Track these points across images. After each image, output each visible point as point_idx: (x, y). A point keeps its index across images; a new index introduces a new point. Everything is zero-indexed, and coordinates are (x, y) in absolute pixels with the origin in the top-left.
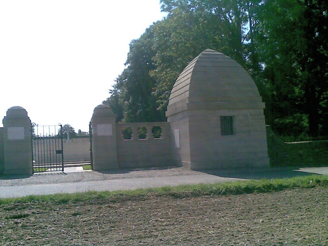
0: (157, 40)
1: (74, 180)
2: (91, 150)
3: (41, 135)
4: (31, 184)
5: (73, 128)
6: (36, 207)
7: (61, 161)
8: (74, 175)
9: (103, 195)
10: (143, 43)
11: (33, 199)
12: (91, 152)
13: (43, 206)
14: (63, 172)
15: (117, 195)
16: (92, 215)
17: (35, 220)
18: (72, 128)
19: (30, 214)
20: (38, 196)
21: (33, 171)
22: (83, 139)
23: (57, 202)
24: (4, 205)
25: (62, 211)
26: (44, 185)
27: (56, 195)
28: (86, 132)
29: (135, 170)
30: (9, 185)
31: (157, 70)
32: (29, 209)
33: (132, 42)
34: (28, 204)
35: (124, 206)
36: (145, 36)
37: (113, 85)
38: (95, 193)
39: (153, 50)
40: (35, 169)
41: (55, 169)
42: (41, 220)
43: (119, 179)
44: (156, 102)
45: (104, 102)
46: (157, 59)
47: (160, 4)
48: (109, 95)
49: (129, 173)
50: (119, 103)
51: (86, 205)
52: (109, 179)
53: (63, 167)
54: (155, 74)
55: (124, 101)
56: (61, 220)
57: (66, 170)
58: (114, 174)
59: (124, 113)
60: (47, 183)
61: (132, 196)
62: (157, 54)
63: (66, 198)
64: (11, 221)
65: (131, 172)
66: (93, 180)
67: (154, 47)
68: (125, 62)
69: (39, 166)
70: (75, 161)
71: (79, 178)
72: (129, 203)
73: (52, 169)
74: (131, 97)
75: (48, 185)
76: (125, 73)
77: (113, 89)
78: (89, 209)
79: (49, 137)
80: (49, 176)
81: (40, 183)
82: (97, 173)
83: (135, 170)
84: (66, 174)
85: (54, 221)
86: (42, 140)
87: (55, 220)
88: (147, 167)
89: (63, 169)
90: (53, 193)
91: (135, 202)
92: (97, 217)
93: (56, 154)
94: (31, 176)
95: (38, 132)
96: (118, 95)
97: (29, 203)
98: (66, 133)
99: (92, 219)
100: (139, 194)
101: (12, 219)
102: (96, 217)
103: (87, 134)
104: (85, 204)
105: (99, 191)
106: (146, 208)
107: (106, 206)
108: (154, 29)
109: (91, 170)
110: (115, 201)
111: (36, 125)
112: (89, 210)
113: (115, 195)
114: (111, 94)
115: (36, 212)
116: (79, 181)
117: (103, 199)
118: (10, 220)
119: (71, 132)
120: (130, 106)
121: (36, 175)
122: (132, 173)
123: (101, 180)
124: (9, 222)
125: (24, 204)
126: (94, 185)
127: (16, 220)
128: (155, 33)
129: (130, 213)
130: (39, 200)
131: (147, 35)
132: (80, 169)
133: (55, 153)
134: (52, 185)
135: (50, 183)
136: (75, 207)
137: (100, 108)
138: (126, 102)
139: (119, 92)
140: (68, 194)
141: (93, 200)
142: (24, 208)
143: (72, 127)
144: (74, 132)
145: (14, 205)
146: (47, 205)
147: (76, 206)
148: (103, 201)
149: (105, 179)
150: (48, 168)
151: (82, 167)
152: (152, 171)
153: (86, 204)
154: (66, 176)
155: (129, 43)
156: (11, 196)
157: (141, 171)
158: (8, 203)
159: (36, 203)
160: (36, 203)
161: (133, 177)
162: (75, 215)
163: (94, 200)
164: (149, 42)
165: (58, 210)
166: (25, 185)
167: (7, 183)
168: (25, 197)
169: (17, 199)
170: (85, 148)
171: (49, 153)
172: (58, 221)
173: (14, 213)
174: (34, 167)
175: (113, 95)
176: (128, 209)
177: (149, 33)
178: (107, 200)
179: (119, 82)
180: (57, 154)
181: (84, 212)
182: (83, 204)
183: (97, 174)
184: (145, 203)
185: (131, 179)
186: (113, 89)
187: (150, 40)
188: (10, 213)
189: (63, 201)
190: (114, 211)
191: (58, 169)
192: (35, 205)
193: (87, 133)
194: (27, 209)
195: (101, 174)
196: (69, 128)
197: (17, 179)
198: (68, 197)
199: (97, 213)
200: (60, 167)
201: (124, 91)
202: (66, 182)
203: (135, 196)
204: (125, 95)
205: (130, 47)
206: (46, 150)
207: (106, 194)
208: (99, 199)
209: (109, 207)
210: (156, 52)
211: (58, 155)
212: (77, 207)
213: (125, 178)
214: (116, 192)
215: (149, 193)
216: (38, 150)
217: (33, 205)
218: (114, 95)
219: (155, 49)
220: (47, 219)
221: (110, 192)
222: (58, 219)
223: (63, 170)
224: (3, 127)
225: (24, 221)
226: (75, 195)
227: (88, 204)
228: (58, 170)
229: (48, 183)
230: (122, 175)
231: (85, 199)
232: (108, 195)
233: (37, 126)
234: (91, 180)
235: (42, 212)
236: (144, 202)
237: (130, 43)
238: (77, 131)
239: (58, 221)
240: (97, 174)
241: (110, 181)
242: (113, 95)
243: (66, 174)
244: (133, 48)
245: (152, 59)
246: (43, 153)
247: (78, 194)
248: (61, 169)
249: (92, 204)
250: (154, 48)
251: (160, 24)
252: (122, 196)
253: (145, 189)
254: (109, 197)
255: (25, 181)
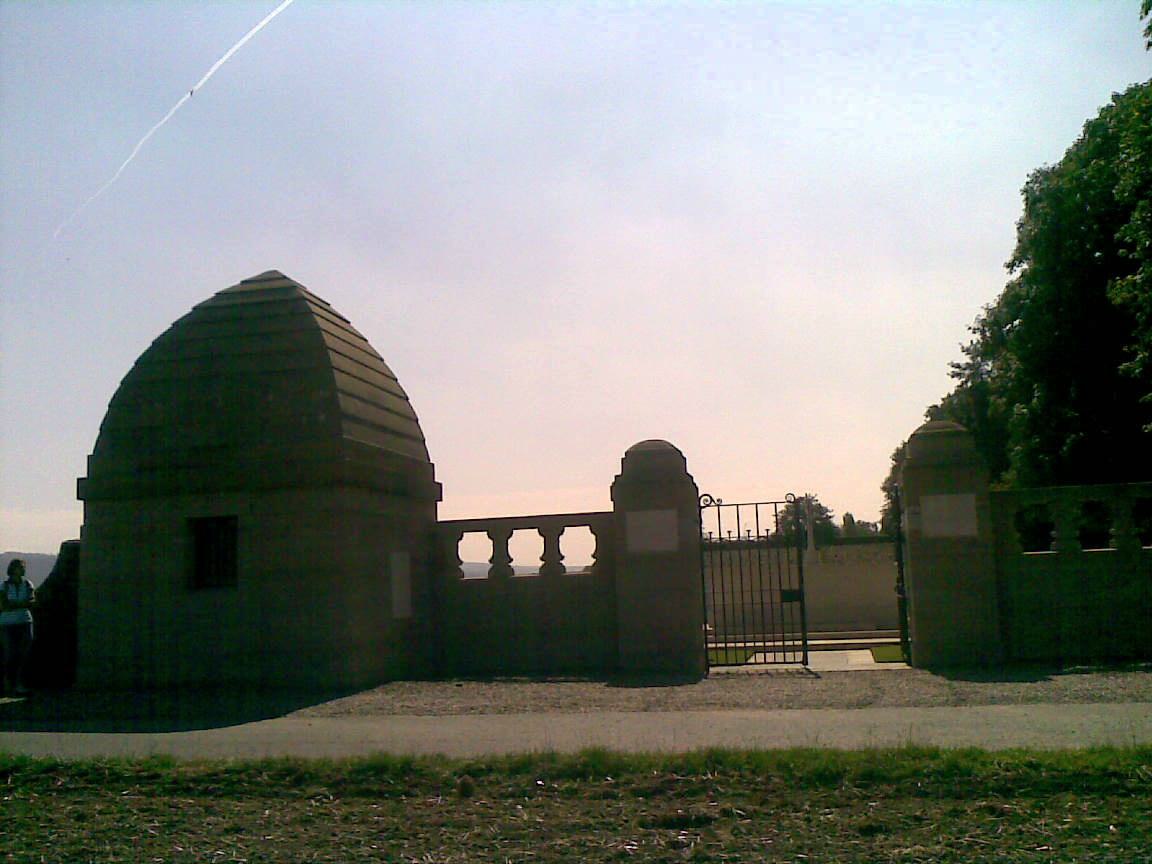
0: (1133, 159)
1: (842, 696)
2: (900, 590)
3: (713, 536)
4: (705, 707)
5: (827, 511)
6: (731, 792)
7: (799, 627)
8: (847, 681)
9: (963, 763)
10: (1079, 178)
11: (720, 763)
12: (899, 598)
13: (755, 790)
14: (807, 667)
15: (1017, 765)
16: (932, 836)
17: (733, 838)
18: (821, 510)
19: (717, 816)
20: (737, 753)
21: (708, 660)
22: (859, 547)
23: (801, 779)
24: (629, 776)
25: (821, 812)
26: (747, 714)
27: (797, 753)
28: (872, 521)
29: (562, 678)
30: (638, 708)
31: (1138, 277)
32: (710, 797)
33: (1032, 181)
34: (705, 778)
35: (1047, 811)
36: (1082, 154)
37: (967, 344)
38: (934, 754)
39: (1119, 201)
40: (712, 655)
41: (780, 657)
42: (754, 840)
43: (1012, 705)
44: (1140, 401)
45: (934, 412)
46: (1137, 230)
47: (1141, 18)
48: (951, 385)
49: (1047, 683)
50: (989, 413)
51: (903, 796)
52: (974, 702)
53: (805, 649)
54: (1130, 292)
55: (1011, 404)
56: (821, 848)
57: (818, 661)
58: (990, 685)
59: (1012, 450)
60: (758, 707)
61: (1077, 775)
62: (1136, 215)
63: (831, 767)
64: (657, 837)
65: (1055, 677)
66: (916, 704)
67: (1122, 190)
68: (1009, 259)
69: (783, 641)
70: (846, 627)
71: (866, 694)
72: (1068, 800)
73: (770, 657)
74: (1035, 386)
75: (762, 712)
76: (1011, 299)
77: (965, 359)
78: (918, 813)
79: (758, 542)
80: (760, 682)
81: (737, 705)
82: (926, 675)
83: (562, 678)
84: (819, 677)
85: (800, 847)
86: (742, 552)
87: (799, 843)
88: (545, 671)
89: (805, 657)
90: (784, 744)
91: (1088, 797)
92: (949, 848)
93: (782, 602)
94: (704, 680)
95: (712, 524)
96: (984, 383)
97: (709, 776)
98: (803, 522)
99: (934, 853)
100: (1104, 770)
101: (661, 830)
102: (947, 845)
103: (873, 529)
104: (899, 795)
105: (946, 747)
106: (1139, 829)
107: (980, 808)
108: (1120, 121)
109: (903, 666)
110: (1010, 790)
111: (713, 504)
112: (917, 819)
113: (1010, 768)
114: (957, 382)
115: (734, 811)
116: (861, 704)
117: (966, 778)
118: (653, 831)
119: (818, 522)
120: (1035, 423)
121: (718, 674)
122: (1060, 681)
123: (945, 704)
124: (651, 838)
125: (694, 779)
126: (925, 724)
127: (672, 833)
128: (1123, 134)
129: (1076, 844)
130: (740, 768)
131: (1091, 148)
132: (862, 659)
133: (777, 599)
134: (774, 715)
135: (767, 704)
136: (866, 801)
137: (932, 435)
138: (1020, 409)
139: (989, 372)
140: (836, 754)
141: (927, 780)
142: (694, 793)
143: (823, 505)
144: (830, 522)
145: (661, 780)
146: (770, 787)
147: (869, 797)
148: (253, 787)
149: (960, 701)
150: (756, 650)
151: (868, 652)
152: (1142, 677)
153: (904, 793)
154: (819, 684)
155: (1023, 185)
156: (652, 750)
157: (1095, 675)
158: (642, 772)
159: (733, 777)
160: (733, 777)
161: (1067, 699)
162: (869, 831)
163: (932, 778)
164: (1100, 170)
165: (806, 807)
166: (687, 709)
167: (629, 699)
168: (694, 756)
169: (671, 758)
170: (879, 581)
171: (757, 599)
172: (811, 850)
173: (663, 808)
174: (710, 645)
175: (966, 382)
176: (1066, 826)
177: (1099, 140)
178: (981, 783)
179: (988, 334)
180: (784, 604)
181: (900, 822)
182: (891, 790)
183: (928, 683)
184: (1131, 807)
185: (1061, 705)
186: (965, 359)
187: (1102, 163)
188: (651, 807)
189: (822, 776)
190: (1012, 830)
191: (790, 656)
192: (729, 785)
193: (875, 525)
194: (704, 797)
195: (940, 679)
196: (812, 511)
197: (660, 688)
198: (840, 764)
199: (950, 833)
200: (794, 649)
201: (1009, 365)
202: (821, 705)
203: (1087, 775)
204: (1012, 380)
205: (1027, 199)
206: (766, 586)
207: (975, 760)
208: (957, 779)
209: (992, 810)
210: (1133, 207)
211: (786, 605)
212: (874, 804)
213: (1035, 700)
214: (1012, 757)
215: (1144, 767)
216: (722, 590)
217: (720, 783)
218: (969, 384)
219: (1126, 194)
220: (775, 838)
221: (989, 755)
222: (809, 842)
223: (805, 662)
224: (612, 510)
225: (699, 840)
226: (863, 757)
227: (910, 793)
228: (787, 660)
229: (762, 707)
230: (1024, 688)
231: (895, 774)
232: (983, 764)
233: (718, 506)
234: (908, 704)
235: (755, 811)
236: (1126, 800)
237: (1027, 183)
238: (838, 521)
239: (811, 850)
240: (928, 683)
241: (979, 708)
242: (966, 382)
243: (817, 676)
244: (1038, 200)
245: (1117, 235)
246: (738, 601)
247: (871, 755)
248: (799, 656)
249: (926, 795)
250: (1123, 191)
251: (1143, 99)
252: (1033, 773)
253: (1127, 750)
254: (985, 773)
255: (686, 694)
